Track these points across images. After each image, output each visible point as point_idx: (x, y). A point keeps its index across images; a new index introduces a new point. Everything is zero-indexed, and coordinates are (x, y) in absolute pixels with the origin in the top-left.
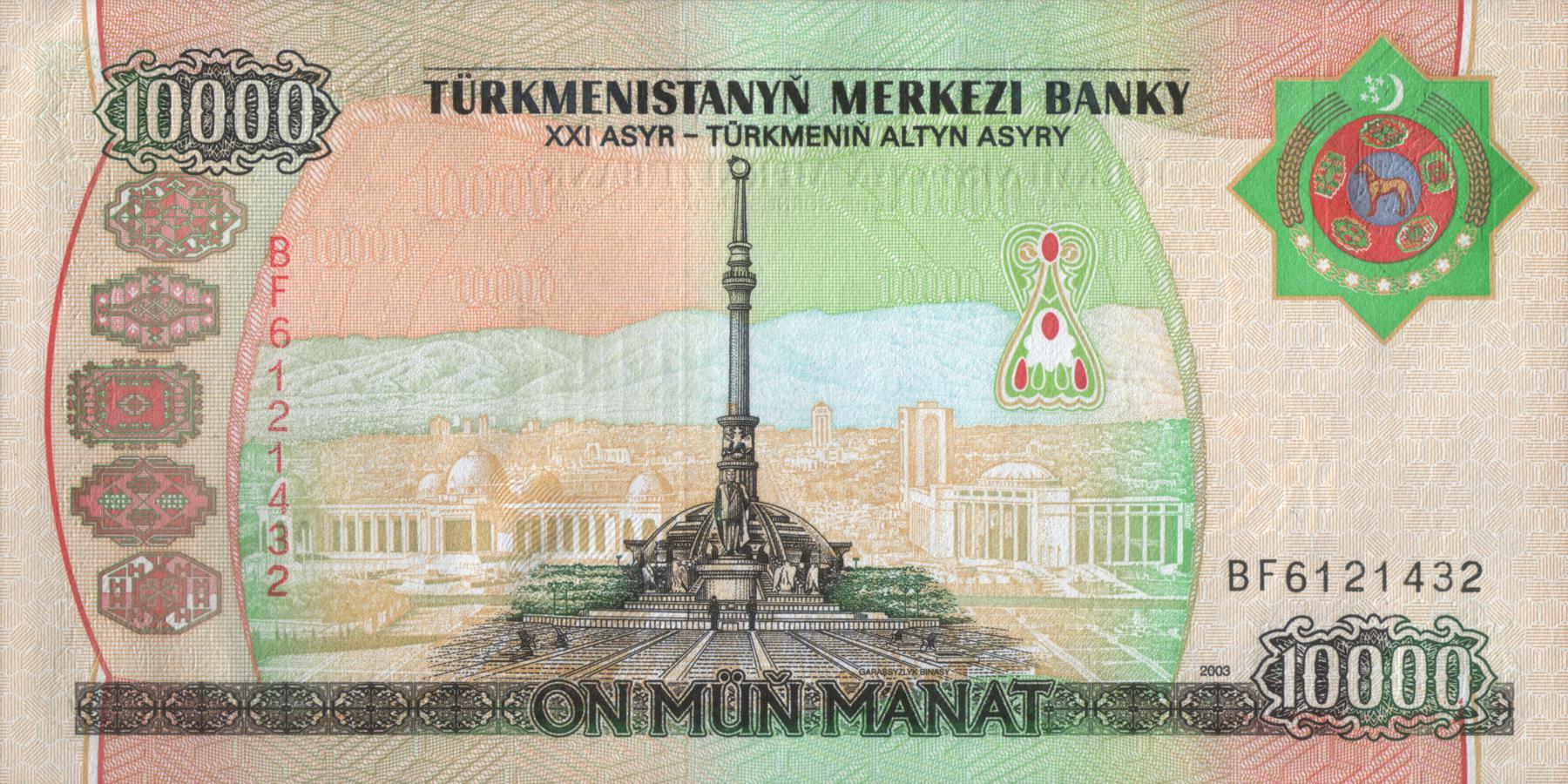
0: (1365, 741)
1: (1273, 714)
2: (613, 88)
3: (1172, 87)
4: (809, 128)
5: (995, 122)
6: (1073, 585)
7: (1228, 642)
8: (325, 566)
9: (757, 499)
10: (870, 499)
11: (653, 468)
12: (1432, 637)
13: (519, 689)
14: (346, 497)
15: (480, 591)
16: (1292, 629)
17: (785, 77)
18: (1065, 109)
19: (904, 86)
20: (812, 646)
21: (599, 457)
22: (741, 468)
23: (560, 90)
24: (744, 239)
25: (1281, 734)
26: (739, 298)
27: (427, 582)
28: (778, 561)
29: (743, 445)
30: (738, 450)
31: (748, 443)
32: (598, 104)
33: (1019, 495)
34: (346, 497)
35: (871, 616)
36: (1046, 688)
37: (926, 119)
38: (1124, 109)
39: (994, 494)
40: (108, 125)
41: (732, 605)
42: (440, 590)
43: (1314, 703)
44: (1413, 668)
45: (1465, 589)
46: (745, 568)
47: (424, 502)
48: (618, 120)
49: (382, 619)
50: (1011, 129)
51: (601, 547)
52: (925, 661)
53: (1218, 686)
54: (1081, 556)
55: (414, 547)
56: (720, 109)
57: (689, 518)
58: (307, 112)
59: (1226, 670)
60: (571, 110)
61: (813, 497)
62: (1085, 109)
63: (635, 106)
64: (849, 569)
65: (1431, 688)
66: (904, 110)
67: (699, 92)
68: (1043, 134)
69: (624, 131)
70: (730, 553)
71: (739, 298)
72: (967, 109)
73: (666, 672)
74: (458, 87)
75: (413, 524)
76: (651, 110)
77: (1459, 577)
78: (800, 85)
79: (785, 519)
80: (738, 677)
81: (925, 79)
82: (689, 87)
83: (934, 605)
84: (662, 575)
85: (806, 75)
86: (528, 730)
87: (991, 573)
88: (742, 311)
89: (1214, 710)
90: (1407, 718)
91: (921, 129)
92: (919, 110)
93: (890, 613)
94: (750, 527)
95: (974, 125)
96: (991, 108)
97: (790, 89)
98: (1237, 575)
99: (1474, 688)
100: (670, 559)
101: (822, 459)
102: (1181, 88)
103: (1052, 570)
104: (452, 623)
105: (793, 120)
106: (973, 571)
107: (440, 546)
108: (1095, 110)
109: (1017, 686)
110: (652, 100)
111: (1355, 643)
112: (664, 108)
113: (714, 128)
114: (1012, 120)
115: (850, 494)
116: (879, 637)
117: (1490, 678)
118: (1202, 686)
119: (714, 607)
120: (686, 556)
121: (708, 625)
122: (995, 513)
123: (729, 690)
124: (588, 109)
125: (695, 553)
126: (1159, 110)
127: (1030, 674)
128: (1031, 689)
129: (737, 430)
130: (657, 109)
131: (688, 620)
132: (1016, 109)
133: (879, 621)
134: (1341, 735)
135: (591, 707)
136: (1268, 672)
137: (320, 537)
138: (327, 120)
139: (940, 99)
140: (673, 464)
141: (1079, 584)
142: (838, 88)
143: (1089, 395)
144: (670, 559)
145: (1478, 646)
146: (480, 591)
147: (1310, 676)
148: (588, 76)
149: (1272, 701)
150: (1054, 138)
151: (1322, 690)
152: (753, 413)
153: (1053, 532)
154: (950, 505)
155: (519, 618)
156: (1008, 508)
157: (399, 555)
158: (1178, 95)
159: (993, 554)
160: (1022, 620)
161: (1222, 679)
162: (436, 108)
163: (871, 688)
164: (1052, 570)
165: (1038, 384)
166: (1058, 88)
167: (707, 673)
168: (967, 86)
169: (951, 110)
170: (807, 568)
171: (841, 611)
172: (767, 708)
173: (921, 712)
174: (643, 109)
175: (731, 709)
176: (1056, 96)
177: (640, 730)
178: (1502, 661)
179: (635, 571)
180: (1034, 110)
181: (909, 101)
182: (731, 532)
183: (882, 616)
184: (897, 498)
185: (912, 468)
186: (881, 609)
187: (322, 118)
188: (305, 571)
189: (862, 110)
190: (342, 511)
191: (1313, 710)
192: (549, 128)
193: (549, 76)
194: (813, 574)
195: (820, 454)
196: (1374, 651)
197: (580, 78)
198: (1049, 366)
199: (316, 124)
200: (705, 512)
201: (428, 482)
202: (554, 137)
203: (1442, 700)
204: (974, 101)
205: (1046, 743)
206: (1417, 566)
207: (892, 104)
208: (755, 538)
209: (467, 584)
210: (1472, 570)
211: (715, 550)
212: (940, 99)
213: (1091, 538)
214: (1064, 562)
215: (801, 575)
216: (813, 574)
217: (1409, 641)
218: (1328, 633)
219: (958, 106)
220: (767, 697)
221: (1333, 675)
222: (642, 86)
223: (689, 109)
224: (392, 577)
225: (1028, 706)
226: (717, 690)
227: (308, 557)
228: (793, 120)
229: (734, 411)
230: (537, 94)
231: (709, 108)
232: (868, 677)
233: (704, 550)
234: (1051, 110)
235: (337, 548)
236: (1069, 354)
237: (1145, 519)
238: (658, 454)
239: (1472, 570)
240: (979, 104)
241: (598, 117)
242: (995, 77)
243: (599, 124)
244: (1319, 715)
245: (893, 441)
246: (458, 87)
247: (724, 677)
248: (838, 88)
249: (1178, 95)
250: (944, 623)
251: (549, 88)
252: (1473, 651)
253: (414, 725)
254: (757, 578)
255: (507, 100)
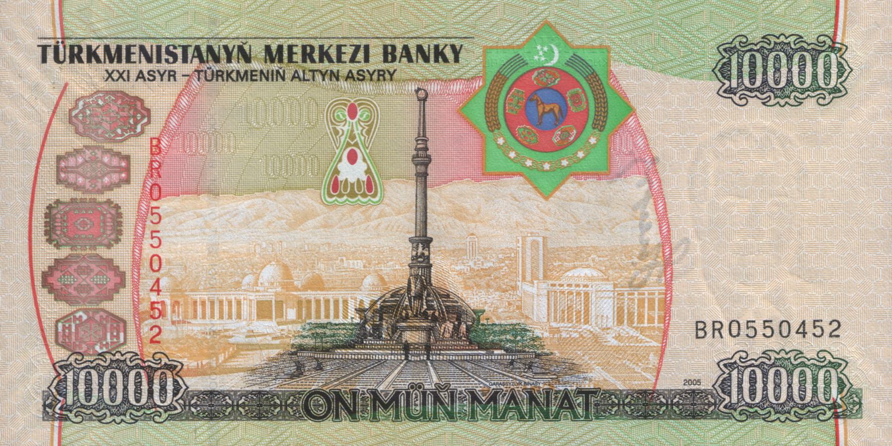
0: (778, 422)
1: (725, 407)
2: (142, 49)
3: (453, 47)
4: (252, 71)
5: (354, 68)
6: (616, 338)
7: (693, 364)
8: (186, 327)
9: (431, 285)
10: (499, 289)
11: (376, 271)
12: (815, 362)
13: (296, 394)
14: (201, 287)
15: (278, 342)
16: (737, 357)
17: (238, 43)
18: (394, 59)
19: (304, 47)
20: (462, 369)
21: (345, 265)
22: (422, 267)
23: (274, 48)
24: (424, 136)
25: (730, 418)
26: (421, 169)
27: (247, 337)
28: (444, 320)
29: (423, 254)
30: (420, 257)
31: (426, 253)
32: (134, 58)
33: (585, 286)
34: (201, 287)
35: (496, 352)
36: (595, 393)
37: (317, 66)
38: (426, 59)
39: (578, 286)
40: (721, 79)
41: (417, 346)
42: (254, 340)
43: (748, 400)
44: (805, 380)
45: (831, 336)
46: (424, 324)
47: (245, 290)
48: (145, 67)
49: (221, 358)
50: (363, 71)
51: (345, 317)
52: (527, 377)
53: (693, 391)
54: (620, 322)
55: (239, 316)
56: (202, 61)
57: (392, 296)
58: (834, 70)
59: (698, 382)
60: (119, 61)
61: (467, 287)
62: (404, 60)
63: (155, 59)
64: (483, 325)
65: (815, 392)
66: (304, 61)
67: (190, 51)
68: (381, 74)
69: (358, 73)
70: (416, 316)
71: (421, 169)
72: (339, 60)
73: (379, 384)
74: (56, 48)
75: (239, 303)
76: (163, 61)
77: (828, 329)
78: (246, 48)
79: (448, 296)
80: (420, 387)
81: (316, 44)
82: (185, 49)
83: (532, 346)
84: (377, 328)
85: (250, 42)
86: (300, 418)
87: (568, 330)
88: (422, 177)
89: (692, 405)
90: (802, 409)
91: (313, 71)
92: (313, 61)
93: (507, 350)
94: (427, 301)
95: (343, 69)
96: (353, 60)
97: (241, 49)
98: (700, 329)
99: (840, 391)
100: (381, 319)
101: (473, 266)
102: (458, 48)
103: (603, 329)
104: (256, 359)
105: (242, 66)
106: (558, 330)
107: (254, 316)
108: (410, 60)
109: (580, 392)
110: (164, 56)
111: (772, 366)
112: (171, 59)
113: (199, 72)
114: (363, 66)
115: (489, 286)
116: (501, 364)
117: (848, 386)
118: (686, 391)
119: (407, 347)
120: (390, 317)
121: (403, 357)
122: (571, 297)
123: (414, 393)
124: (128, 60)
125: (396, 316)
126: (446, 60)
127: (587, 385)
128: (587, 393)
129: (420, 245)
130: (167, 61)
131: (392, 354)
132: (367, 60)
133: (501, 355)
134: (764, 419)
135: (338, 405)
136: (722, 383)
137: (186, 312)
138: (846, 74)
139: (324, 55)
140: (386, 270)
141: (618, 337)
142: (268, 49)
143: (374, 196)
144: (381, 319)
145: (842, 367)
146: (278, 342)
147: (746, 385)
148: (290, 42)
149: (724, 399)
150: (387, 76)
151: (753, 392)
152: (429, 235)
153: (604, 308)
154: (545, 292)
155: (295, 353)
156: (578, 294)
157: (230, 321)
158: (456, 52)
159: (570, 320)
160: (586, 358)
161: (696, 387)
162: (44, 60)
163: (496, 393)
164: (603, 329)
165: (345, 190)
166: (308, 48)
167: (404, 386)
168: (339, 47)
169: (330, 61)
170: (460, 324)
171: (479, 349)
172: (439, 404)
173: (525, 408)
174: (159, 61)
175: (416, 405)
176: (389, 54)
177: (364, 418)
178: (855, 375)
179: (362, 326)
180: (376, 62)
181: (307, 55)
182: (416, 304)
183: (503, 352)
184: (514, 288)
185: (524, 271)
186: (500, 348)
187: (843, 74)
188: (177, 330)
189: (281, 61)
190: (198, 297)
191: (748, 405)
192: (107, 71)
193: (107, 42)
194: (463, 327)
195: (471, 263)
196: (783, 371)
197: (124, 44)
198: (352, 179)
199: (839, 77)
200: (402, 292)
201: (249, 279)
202: (110, 75)
203: (821, 396)
204: (294, 56)
205: (594, 424)
206: (803, 323)
207: (298, 58)
208: (430, 307)
209: (269, 338)
210: (835, 325)
211: (407, 314)
212: (324, 55)
213: (626, 311)
214: (610, 325)
215: (456, 329)
216: (463, 327)
217: (803, 364)
218: (756, 361)
219: (334, 58)
220: (437, 399)
221: (759, 385)
222: (159, 48)
223: (185, 60)
224: (227, 334)
225: (597, 403)
226: (408, 394)
227: (179, 322)
228: (242, 66)
229: (418, 234)
230: (101, 53)
231: (196, 61)
232: (494, 387)
233: (401, 314)
234: (386, 60)
235: (195, 317)
236: (364, 174)
237: (657, 299)
238: (379, 263)
239: (835, 325)
240: (346, 58)
241: (344, 65)
242: (356, 42)
243: (134, 69)
244: (751, 407)
245: (513, 255)
246: (56, 48)
247: (412, 387)
248: (268, 49)
249: (456, 52)
250: (538, 356)
251: (107, 48)
252: (839, 370)
253: (234, 416)
254: (429, 331)
255: (84, 56)
